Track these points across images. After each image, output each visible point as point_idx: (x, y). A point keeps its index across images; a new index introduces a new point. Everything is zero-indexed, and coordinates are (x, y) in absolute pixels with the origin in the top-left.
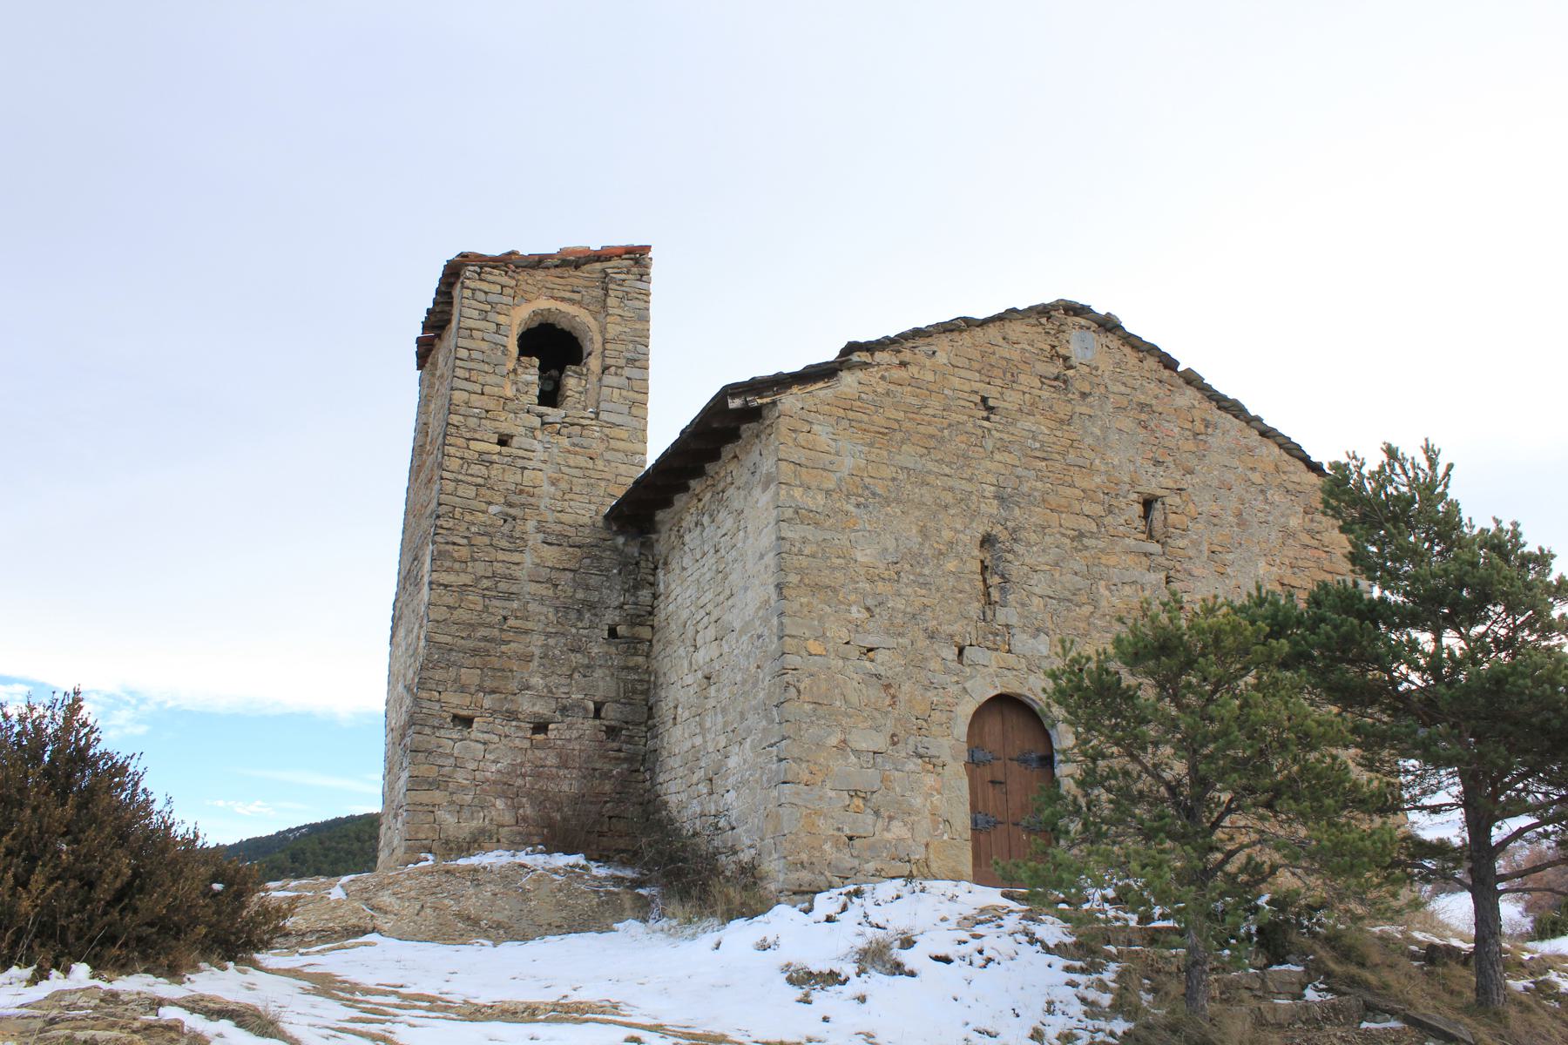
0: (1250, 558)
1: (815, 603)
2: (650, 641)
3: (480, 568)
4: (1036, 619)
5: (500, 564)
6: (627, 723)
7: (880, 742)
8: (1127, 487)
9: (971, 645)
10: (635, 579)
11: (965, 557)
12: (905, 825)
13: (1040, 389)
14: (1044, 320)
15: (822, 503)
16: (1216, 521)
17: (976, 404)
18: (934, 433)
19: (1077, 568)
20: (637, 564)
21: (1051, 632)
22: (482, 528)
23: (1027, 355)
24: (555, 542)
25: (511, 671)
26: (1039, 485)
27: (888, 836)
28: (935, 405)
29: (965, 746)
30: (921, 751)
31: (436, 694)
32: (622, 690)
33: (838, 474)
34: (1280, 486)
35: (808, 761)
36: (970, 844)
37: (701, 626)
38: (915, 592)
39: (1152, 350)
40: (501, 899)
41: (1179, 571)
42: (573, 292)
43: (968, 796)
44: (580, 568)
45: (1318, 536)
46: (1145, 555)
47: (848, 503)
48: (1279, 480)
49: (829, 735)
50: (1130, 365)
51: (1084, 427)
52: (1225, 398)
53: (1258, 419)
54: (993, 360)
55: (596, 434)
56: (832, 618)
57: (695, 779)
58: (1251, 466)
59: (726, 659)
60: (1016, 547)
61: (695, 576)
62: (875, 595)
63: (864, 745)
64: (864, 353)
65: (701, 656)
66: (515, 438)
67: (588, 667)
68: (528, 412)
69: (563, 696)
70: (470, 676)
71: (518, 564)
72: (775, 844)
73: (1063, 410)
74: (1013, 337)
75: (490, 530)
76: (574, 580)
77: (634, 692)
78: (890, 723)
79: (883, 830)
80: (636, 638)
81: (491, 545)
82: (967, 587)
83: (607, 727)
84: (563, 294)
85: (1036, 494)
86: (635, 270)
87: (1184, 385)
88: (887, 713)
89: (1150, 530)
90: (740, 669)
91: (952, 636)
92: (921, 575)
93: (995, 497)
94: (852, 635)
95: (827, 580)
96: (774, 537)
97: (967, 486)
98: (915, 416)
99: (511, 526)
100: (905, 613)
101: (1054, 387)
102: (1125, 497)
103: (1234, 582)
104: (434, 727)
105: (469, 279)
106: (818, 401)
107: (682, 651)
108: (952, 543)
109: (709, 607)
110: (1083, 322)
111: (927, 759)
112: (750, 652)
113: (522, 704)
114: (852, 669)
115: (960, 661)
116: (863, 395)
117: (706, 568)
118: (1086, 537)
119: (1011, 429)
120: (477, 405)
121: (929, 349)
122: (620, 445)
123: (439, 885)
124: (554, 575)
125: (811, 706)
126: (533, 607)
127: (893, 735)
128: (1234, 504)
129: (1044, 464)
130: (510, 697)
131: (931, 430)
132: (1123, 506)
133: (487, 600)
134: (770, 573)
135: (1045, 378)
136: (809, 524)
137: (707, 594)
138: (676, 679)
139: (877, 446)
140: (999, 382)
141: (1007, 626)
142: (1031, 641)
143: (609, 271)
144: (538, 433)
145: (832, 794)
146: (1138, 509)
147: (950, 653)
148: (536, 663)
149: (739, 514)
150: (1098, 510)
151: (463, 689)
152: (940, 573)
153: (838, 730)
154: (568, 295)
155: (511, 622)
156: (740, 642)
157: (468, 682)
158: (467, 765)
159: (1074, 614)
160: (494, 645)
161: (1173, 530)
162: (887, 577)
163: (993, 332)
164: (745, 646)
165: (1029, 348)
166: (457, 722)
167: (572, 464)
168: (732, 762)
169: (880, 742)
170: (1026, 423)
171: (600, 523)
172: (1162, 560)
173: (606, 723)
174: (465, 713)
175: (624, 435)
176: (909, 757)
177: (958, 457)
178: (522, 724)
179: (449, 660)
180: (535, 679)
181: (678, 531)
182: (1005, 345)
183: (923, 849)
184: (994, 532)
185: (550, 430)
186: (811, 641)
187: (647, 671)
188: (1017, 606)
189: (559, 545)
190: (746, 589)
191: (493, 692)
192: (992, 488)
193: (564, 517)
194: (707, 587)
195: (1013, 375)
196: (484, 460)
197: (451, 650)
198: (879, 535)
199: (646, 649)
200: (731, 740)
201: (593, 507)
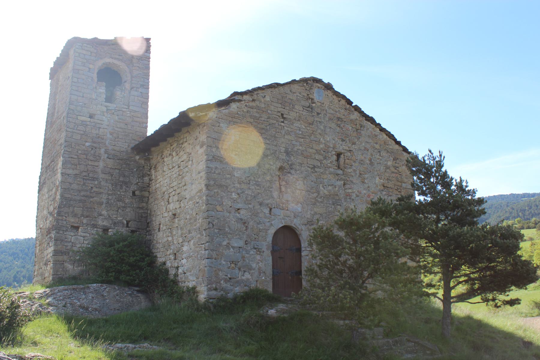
0: (373, 176)
1: (219, 192)
2: (148, 197)
4: (297, 198)
5: (90, 166)
6: (139, 229)
7: (241, 243)
8: (332, 149)
9: (274, 208)
10: (143, 173)
11: (273, 175)
13: (303, 111)
14: (305, 84)
16: (362, 162)
17: (279, 116)
19: (312, 179)
22: (83, 151)
23: (299, 97)
25: (94, 209)
26: (300, 148)
27: (244, 278)
28: (264, 117)
29: (271, 245)
30: (256, 247)
31: (65, 218)
32: (137, 216)
34: (385, 150)
36: (272, 280)
37: (171, 195)
38: (255, 188)
39: (344, 97)
40: (95, 299)
41: (348, 181)
42: (120, 56)
44: (121, 168)
45: (398, 169)
46: (337, 174)
48: (385, 148)
49: (223, 241)
50: (335, 103)
52: (368, 116)
53: (379, 124)
56: (226, 198)
57: (168, 253)
58: (376, 142)
59: (183, 209)
60: (291, 171)
61: (169, 175)
62: (241, 189)
64: (240, 96)
65: (171, 206)
67: (124, 207)
68: (101, 105)
69: (115, 218)
71: (97, 166)
72: (203, 281)
73: (310, 120)
74: (294, 91)
75: (86, 152)
77: (142, 217)
78: (245, 236)
79: (242, 276)
80: (142, 196)
81: (87, 158)
83: (131, 230)
85: (299, 151)
87: (354, 111)
89: (339, 165)
90: (188, 214)
91: (268, 205)
92: (257, 181)
93: (285, 152)
95: (224, 183)
96: (205, 166)
97: (275, 148)
100: (251, 196)
101: (308, 110)
102: (331, 153)
103: (367, 185)
104: (64, 231)
107: (162, 203)
109: (175, 188)
110: (319, 85)
112: (193, 208)
113: (98, 222)
114: (232, 216)
115: (270, 214)
117: (174, 173)
118: (316, 168)
119: (291, 126)
122: (138, 119)
123: (71, 294)
125: (217, 230)
126: (103, 183)
127: (246, 241)
128: (369, 157)
129: (303, 140)
130: (94, 219)
131: (263, 126)
132: (330, 156)
134: (203, 179)
135: (305, 107)
136: (218, 162)
137: (174, 183)
138: (160, 214)
140: (288, 108)
141: (287, 201)
145: (224, 263)
146: (335, 157)
147: (267, 211)
148: (104, 205)
149: (189, 155)
150: (321, 157)
151: (75, 215)
152: (264, 181)
153: (227, 239)
155: (95, 189)
156: (189, 204)
158: (77, 245)
159: (311, 196)
161: (347, 166)
162: (245, 182)
163: (286, 87)
164: (191, 206)
165: (299, 95)
166: (72, 228)
168: (185, 248)
169: (241, 243)
170: (297, 124)
171: (129, 151)
172: (343, 177)
173: (131, 229)
174: (76, 225)
175: (140, 116)
176: (251, 249)
179: (70, 204)
181: (161, 156)
182: (291, 94)
183: (255, 282)
184: (284, 166)
186: (218, 206)
187: (147, 209)
188: (291, 193)
189: (113, 159)
190: (192, 184)
191: (87, 217)
192: (284, 149)
193: (115, 148)
194: (174, 180)
195: (293, 105)
197: (71, 200)
199: (146, 200)
200: (184, 240)
201: (127, 144)
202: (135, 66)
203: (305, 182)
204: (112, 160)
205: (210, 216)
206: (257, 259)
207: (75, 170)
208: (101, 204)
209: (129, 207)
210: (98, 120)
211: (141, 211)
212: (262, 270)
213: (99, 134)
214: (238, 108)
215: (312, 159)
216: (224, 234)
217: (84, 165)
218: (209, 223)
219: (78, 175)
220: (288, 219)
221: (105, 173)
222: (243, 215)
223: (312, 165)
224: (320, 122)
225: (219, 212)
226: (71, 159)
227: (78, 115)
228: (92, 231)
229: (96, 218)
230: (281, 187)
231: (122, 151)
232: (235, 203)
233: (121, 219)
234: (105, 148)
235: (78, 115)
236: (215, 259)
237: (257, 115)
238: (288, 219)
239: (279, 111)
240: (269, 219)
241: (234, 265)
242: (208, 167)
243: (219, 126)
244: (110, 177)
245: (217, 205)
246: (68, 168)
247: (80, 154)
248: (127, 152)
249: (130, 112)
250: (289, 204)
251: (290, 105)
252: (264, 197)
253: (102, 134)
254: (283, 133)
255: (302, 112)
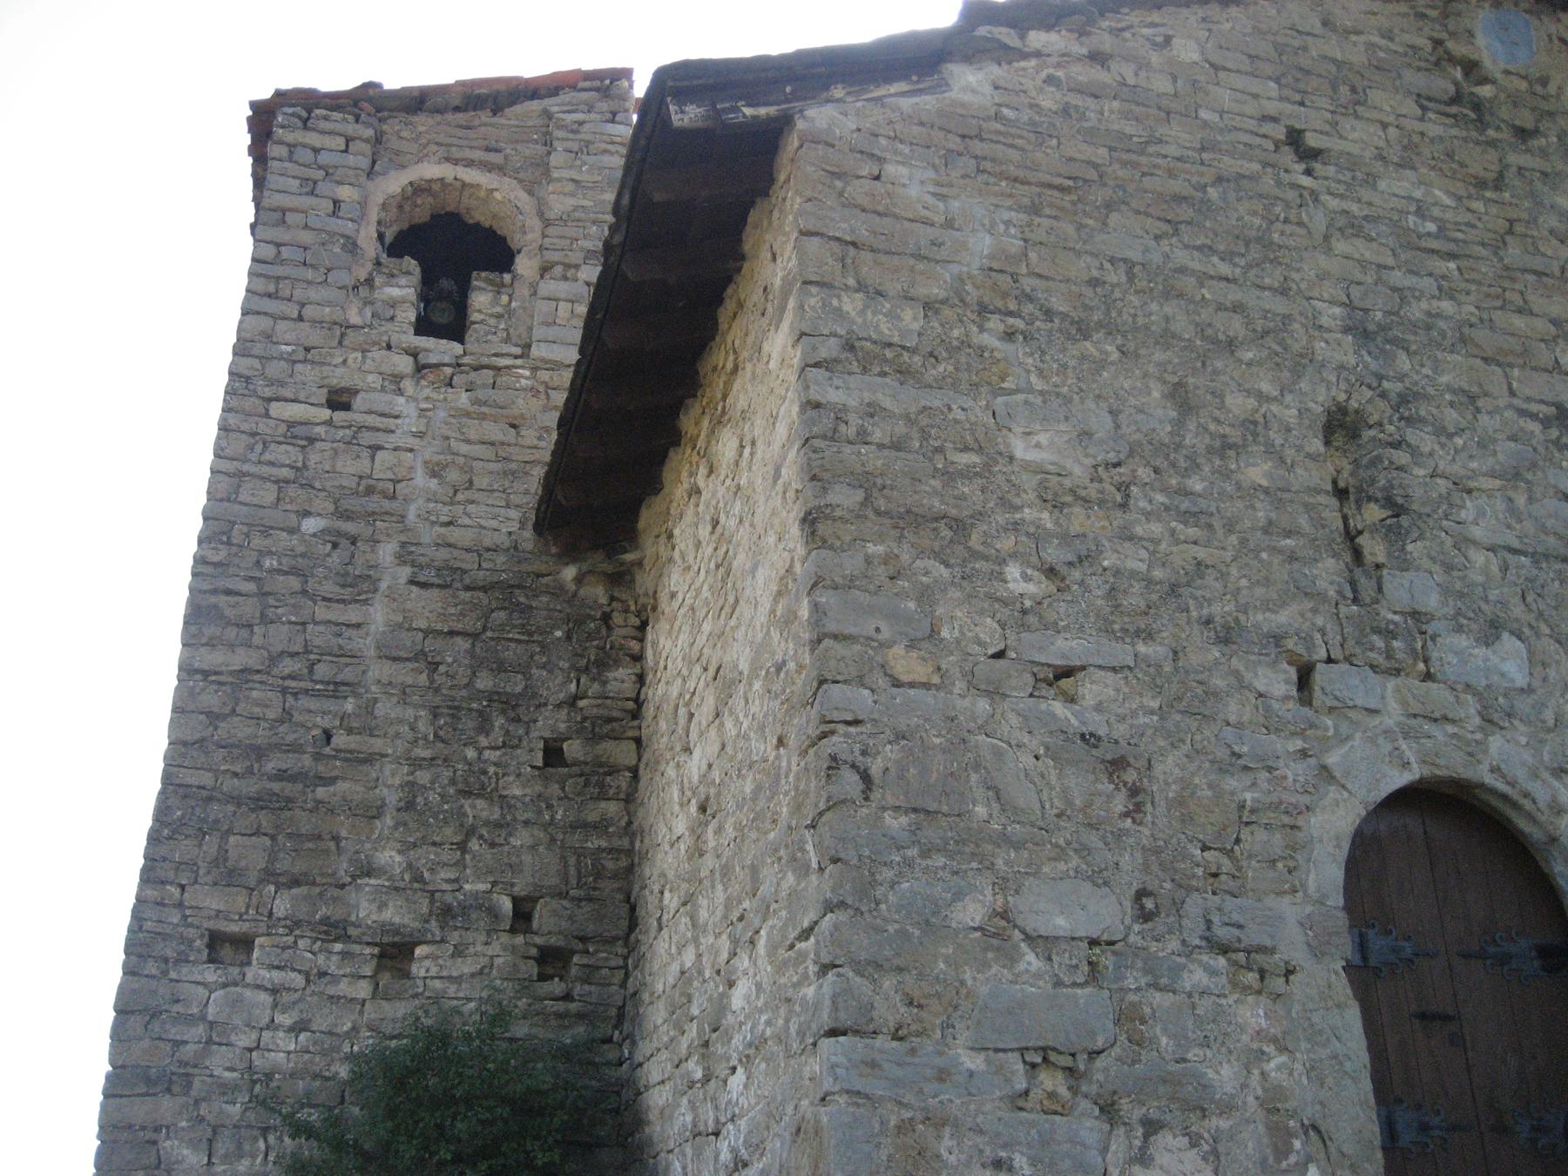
1: (905, 557)
3: (279, 636)
5: (321, 628)
6: (583, 939)
9: (1329, 660)
11: (1290, 453)
12: (1193, 1145)
13: (1422, 119)
15: (916, 326)
18: (1185, 193)
20: (606, 618)
21: (1527, 631)
22: (285, 560)
23: (1382, 54)
24: (436, 581)
25: (336, 839)
26: (1446, 306)
29: (1342, 919)
30: (1222, 933)
31: (174, 891)
32: (572, 871)
33: (955, 268)
35: (900, 970)
42: (488, 149)
43: (1365, 1057)
44: (485, 629)
47: (982, 329)
49: (959, 895)
51: (1532, 195)
54: (1305, 62)
55: (523, 381)
60: (1412, 435)
62: (1066, 539)
63: (1061, 921)
66: (359, 397)
67: (498, 825)
68: (389, 347)
70: (249, 853)
71: (358, 626)
76: (471, 653)
79: (1131, 1161)
80: (601, 765)
81: (304, 592)
82: (1303, 522)
83: (539, 948)
84: (468, 154)
85: (1442, 324)
86: (604, 106)
88: (1120, 835)
91: (1277, 639)
92: (1187, 493)
93: (1346, 330)
94: (1012, 638)
97: (1279, 306)
98: (1134, 157)
99: (347, 553)
100: (1149, 582)
101: (1454, 116)
104: (166, 960)
105: (283, 127)
106: (895, 116)
108: (1255, 423)
111: (1241, 957)
114: (1014, 720)
116: (1005, 111)
119: (1365, 194)
120: (289, 337)
121: (1157, 34)
124: (430, 644)
125: (904, 820)
127: (1141, 894)
129: (1452, 265)
131: (1178, 186)
133: (290, 699)
135: (1429, 99)
136: (883, 374)
139: (1047, 211)
141: (1415, 614)
142: (1480, 652)
143: (555, 109)
144: (408, 385)
147: (1278, 682)
151: (230, 877)
153: (985, 883)
154: (478, 155)
157: (243, 863)
158: (233, 1038)
160: (300, 786)
162: (1094, 495)
165: (1383, 42)
167: (473, 436)
173: (538, 940)
174: (233, 928)
176: (1189, 951)
177: (1247, 245)
178: (356, 948)
179: (204, 820)
180: (387, 854)
184: (1354, 404)
185: (431, 377)
186: (899, 650)
188: (1436, 568)
191: (295, 882)
192: (1337, 310)
193: (454, 535)
195: (1353, 90)
196: (305, 439)
198: (1068, 401)
199: (624, 785)
202: (559, 180)
203: (1521, 500)
204: (434, 593)
205: (836, 716)
206: (1242, 1029)
207: (241, 651)
208: (375, 812)
209: (526, 823)
210: (370, 412)
211: (594, 843)
212: (1293, 1114)
213: (370, 477)
214: (997, 88)
215: (1535, 369)
216: (964, 842)
217: (291, 623)
218: (835, 763)
219: (258, 672)
220: (1440, 737)
221: (394, 654)
222: (1099, 708)
223: (1542, 402)
224: (1545, 174)
225: (912, 692)
226: (223, 598)
227: (270, 400)
228: (321, 959)
229: (343, 886)
230: (1360, 540)
231: (488, 550)
232: (1028, 629)
233: (482, 887)
234: (403, 538)
235: (270, 400)
236: (896, 1037)
237: (1129, 130)
238: (1440, 737)
239: (1272, 113)
240: (1301, 734)
241: (1060, 1075)
242: (817, 406)
243: (877, 178)
244: (424, 677)
245: (888, 645)
246: (204, 641)
247: (272, 571)
248: (516, 548)
249: (534, 369)
250: (1433, 638)
251: (1335, 88)
252: (1244, 592)
253: (390, 475)
254: (1319, 222)
255: (1418, 126)
